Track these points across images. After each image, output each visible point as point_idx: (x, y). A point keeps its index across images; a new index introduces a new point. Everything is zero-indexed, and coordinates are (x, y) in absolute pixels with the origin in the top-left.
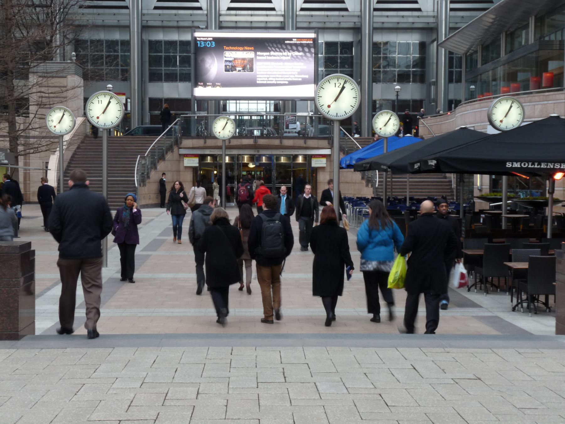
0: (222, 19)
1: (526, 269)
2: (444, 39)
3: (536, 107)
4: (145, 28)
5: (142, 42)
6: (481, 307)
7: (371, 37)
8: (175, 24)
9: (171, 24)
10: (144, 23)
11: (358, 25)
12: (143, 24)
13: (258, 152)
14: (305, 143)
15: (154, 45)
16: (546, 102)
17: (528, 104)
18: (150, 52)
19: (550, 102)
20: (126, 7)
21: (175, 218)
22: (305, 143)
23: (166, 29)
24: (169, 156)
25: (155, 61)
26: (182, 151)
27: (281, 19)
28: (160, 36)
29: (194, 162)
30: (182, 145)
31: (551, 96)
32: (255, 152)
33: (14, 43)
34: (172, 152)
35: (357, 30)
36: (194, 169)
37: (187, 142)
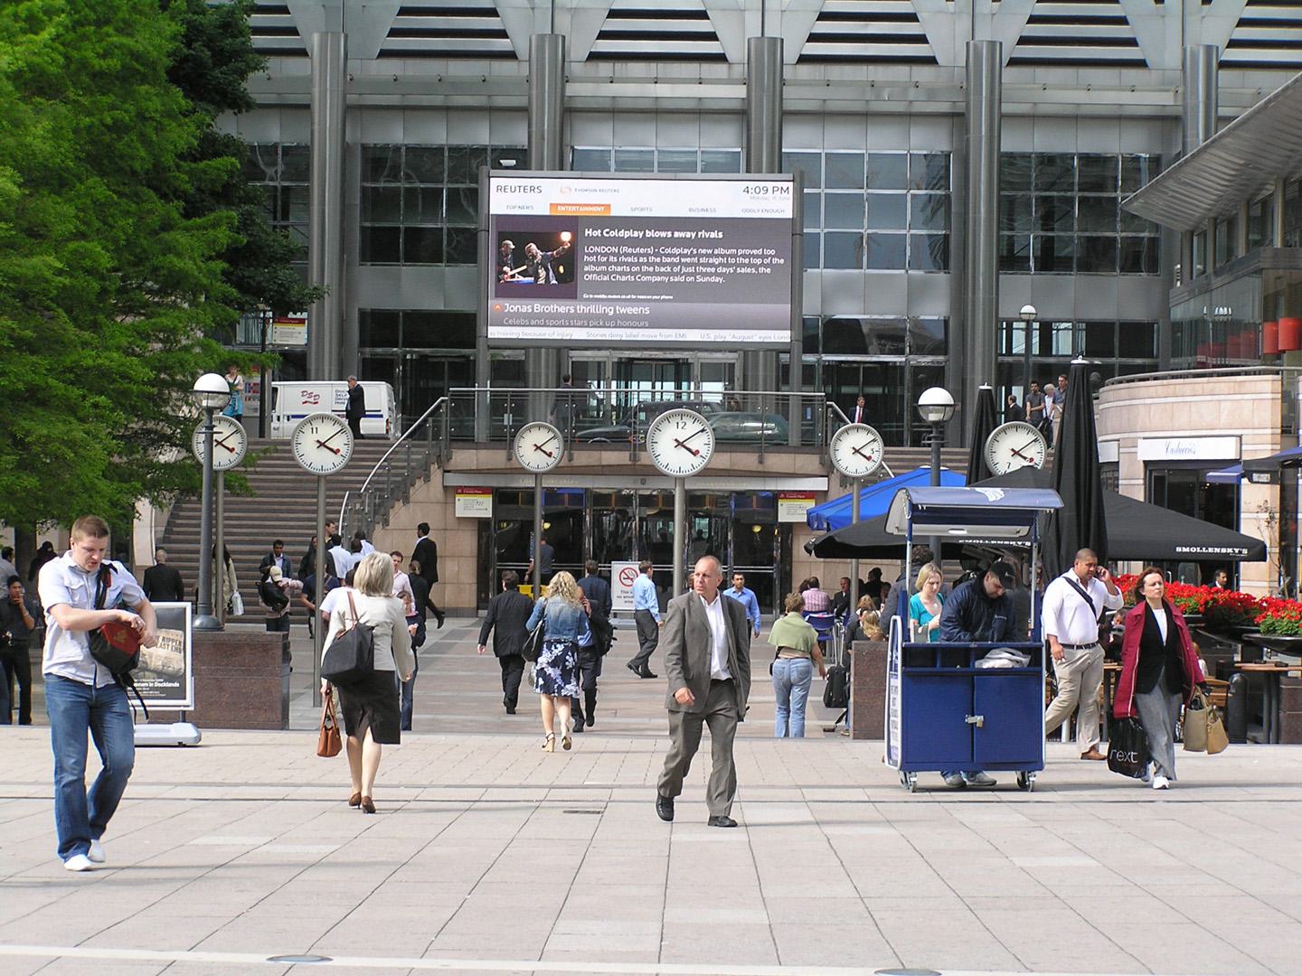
0: (571, 89)
1: (16, 531)
2: (1202, 144)
3: (1223, 404)
4: (352, 111)
5: (346, 150)
6: (825, 730)
7: (994, 138)
8: (438, 100)
9: (425, 100)
10: (353, 99)
11: (961, 108)
12: (348, 102)
13: (643, 482)
14: (761, 462)
15: (378, 160)
16: (1239, 397)
17: (1209, 398)
18: (364, 179)
19: (1246, 397)
20: (302, 53)
21: (660, 589)
22: (761, 462)
23: (408, 113)
24: (419, 491)
25: (376, 202)
26: (454, 480)
27: (741, 92)
28: (396, 134)
29: (482, 507)
30: (452, 465)
31: (1247, 384)
32: (635, 482)
33: (369, 494)
34: (427, 479)
35: (957, 119)
36: (482, 524)
37: (463, 457)
